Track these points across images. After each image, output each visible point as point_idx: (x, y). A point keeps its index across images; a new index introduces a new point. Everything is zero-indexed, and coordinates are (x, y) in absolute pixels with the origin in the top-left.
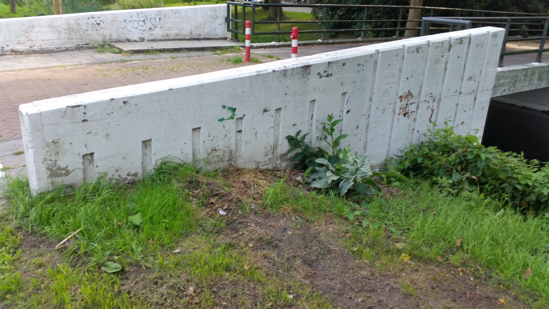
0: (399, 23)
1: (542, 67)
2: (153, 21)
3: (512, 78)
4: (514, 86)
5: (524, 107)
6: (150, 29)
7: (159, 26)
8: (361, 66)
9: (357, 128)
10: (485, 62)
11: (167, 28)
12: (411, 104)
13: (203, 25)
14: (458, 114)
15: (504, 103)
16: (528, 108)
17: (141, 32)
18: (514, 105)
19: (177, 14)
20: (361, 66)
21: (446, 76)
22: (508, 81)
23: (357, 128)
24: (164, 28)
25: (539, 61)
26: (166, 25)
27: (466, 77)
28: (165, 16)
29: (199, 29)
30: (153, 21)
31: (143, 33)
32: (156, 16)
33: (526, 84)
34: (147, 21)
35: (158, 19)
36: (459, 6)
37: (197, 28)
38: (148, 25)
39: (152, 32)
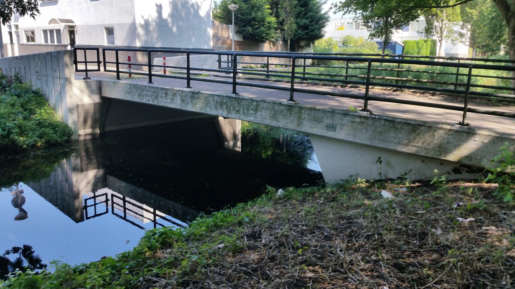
3: (154, 92)
4: (157, 99)
22: (150, 93)
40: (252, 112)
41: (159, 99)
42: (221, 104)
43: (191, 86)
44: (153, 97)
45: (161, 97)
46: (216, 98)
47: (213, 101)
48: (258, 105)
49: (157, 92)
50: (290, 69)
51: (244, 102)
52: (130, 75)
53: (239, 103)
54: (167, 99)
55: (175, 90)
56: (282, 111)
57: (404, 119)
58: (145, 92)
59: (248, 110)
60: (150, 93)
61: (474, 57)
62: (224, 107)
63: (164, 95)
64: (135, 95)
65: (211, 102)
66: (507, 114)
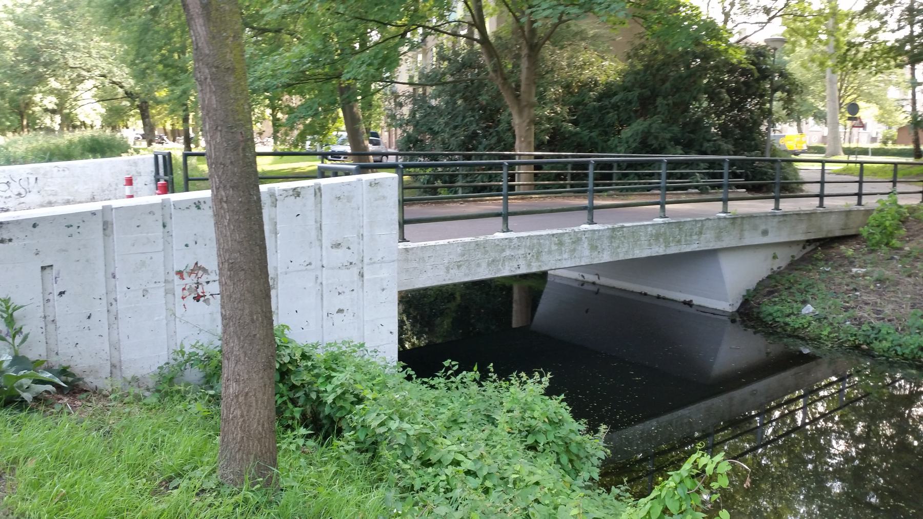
0: (614, 176)
1: (594, 231)
2: (23, 183)
3: (531, 248)
4: (538, 259)
5: (658, 297)
6: (19, 194)
7: (35, 190)
8: (75, 227)
9: (89, 317)
10: (366, 220)
11: (50, 192)
12: (208, 282)
13: (114, 187)
14: (325, 296)
15: (632, 292)
16: (664, 298)
17: (3, 200)
18: (645, 294)
19: (67, 172)
20: (75, 227)
21: (279, 242)
22: (522, 251)
23: (89, 317)
24: (43, 193)
25: (591, 222)
26: (46, 188)
27: (326, 243)
28: (45, 175)
29: (107, 192)
30: (23, 183)
31: (6, 200)
32: (29, 176)
33: (566, 256)
34: (12, 184)
35: (32, 180)
36: (600, 149)
37: (103, 191)
38: (15, 188)
39: (22, 200)
40: (695, 237)
41: (545, 257)
42: (657, 237)
43: (595, 221)
44: (529, 257)
45: (550, 252)
46: (650, 229)
47: (646, 236)
48: (703, 225)
49: (540, 244)
50: (866, 188)
51: (687, 227)
52: (663, 208)
53: (680, 229)
54: (561, 254)
55: (577, 233)
56: (726, 227)
57: (621, 290)
58: (508, 253)
59: (691, 235)
60: (522, 251)
61: (865, 172)
62: (661, 240)
63: (554, 247)
64: (479, 265)
65: (643, 238)
66: (273, 175)
